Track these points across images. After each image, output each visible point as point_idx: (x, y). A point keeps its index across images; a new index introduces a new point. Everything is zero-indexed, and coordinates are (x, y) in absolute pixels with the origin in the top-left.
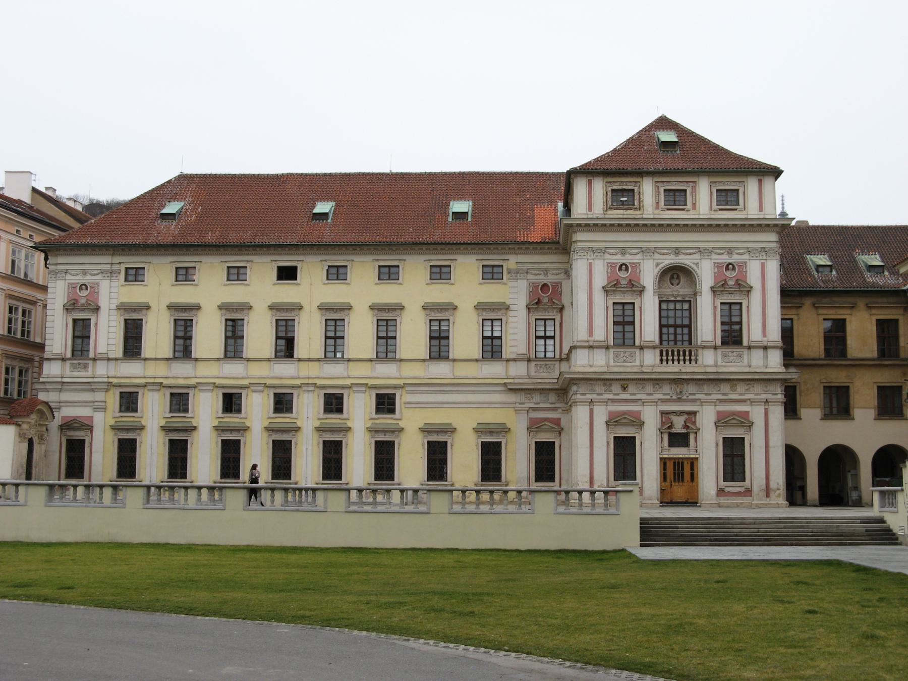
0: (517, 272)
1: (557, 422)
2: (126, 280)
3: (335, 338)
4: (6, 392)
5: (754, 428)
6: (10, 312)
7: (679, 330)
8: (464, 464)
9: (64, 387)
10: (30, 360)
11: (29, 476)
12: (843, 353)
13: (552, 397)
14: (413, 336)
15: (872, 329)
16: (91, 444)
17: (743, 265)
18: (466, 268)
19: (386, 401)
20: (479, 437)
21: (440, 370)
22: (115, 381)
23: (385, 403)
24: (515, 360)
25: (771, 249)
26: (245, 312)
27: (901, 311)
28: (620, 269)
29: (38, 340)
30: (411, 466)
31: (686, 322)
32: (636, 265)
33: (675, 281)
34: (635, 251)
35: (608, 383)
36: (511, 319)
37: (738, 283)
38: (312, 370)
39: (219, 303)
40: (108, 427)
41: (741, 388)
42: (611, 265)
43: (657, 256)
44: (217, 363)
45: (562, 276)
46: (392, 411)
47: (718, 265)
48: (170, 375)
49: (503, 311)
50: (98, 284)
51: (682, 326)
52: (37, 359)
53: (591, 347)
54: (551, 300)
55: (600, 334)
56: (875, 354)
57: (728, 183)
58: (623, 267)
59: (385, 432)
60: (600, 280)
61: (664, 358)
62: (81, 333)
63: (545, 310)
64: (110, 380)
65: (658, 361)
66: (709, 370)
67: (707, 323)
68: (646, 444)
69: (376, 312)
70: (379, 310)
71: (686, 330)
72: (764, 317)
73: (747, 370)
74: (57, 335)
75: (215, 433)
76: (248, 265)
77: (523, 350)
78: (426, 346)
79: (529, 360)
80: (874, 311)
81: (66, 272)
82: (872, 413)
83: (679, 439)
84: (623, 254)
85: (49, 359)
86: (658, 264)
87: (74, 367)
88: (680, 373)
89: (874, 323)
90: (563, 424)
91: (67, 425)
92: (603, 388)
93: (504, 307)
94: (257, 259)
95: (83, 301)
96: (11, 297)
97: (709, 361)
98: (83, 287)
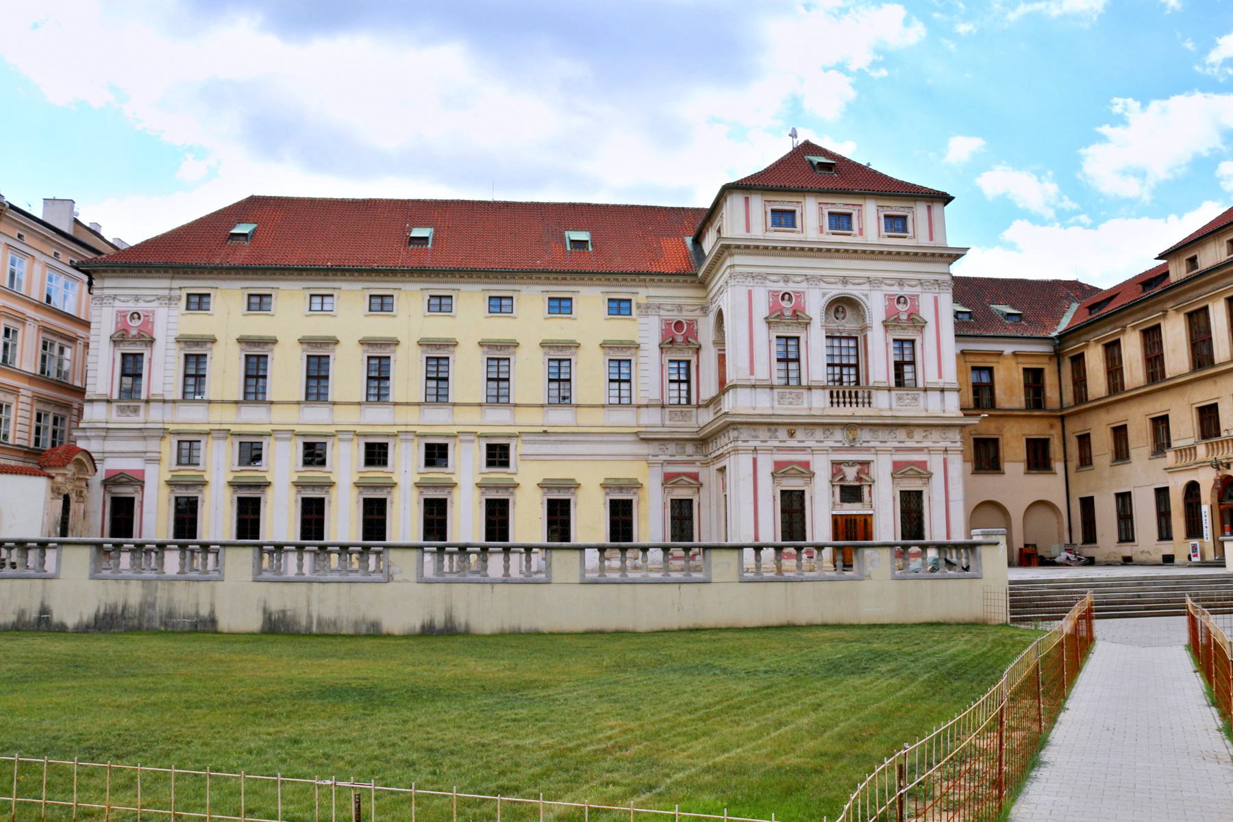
0: (648, 307)
1: (695, 476)
2: (187, 309)
3: (438, 379)
4: (37, 441)
5: (817, 479)
6: (45, 348)
7: (845, 371)
8: (589, 522)
9: (110, 434)
10: (67, 406)
11: (64, 533)
12: (992, 404)
13: (690, 449)
14: (530, 376)
15: (1019, 377)
16: (142, 503)
17: (914, 298)
18: (590, 300)
19: (498, 452)
20: (607, 494)
21: (560, 417)
22: (172, 427)
23: (498, 455)
24: (647, 406)
25: (944, 282)
26: (331, 347)
27: (1046, 360)
28: (783, 299)
29: (78, 384)
30: (528, 523)
31: (853, 361)
32: (799, 294)
33: (840, 315)
34: (798, 279)
35: (773, 428)
36: (641, 360)
37: (910, 319)
38: (410, 417)
39: (300, 337)
40: (162, 483)
41: (918, 434)
42: (774, 294)
43: (823, 285)
44: (296, 407)
45: (698, 313)
46: (506, 464)
47: (889, 298)
48: (238, 421)
49: (633, 351)
50: (153, 312)
51: (849, 366)
52: (76, 406)
53: (754, 386)
54: (687, 341)
55: (762, 373)
56: (1023, 405)
57: (896, 207)
58: (786, 296)
59: (497, 487)
60: (762, 309)
61: (835, 400)
62: (132, 368)
63: (680, 350)
64: (166, 426)
65: (828, 404)
66: (884, 414)
67: (879, 367)
68: (817, 498)
69: (486, 349)
70: (489, 346)
71: (853, 371)
72: (941, 356)
73: (924, 414)
74: (101, 371)
75: (294, 490)
76: (335, 293)
77: (655, 395)
78: (561, 386)
79: (663, 407)
80: (1020, 360)
81: (114, 298)
82: (1022, 467)
83: (851, 493)
84: (786, 281)
85: (91, 401)
86: (824, 295)
87: (122, 410)
88: (853, 416)
89: (1021, 371)
90: (701, 479)
91: (112, 480)
92: (769, 434)
93: (634, 346)
94: (345, 286)
95: (134, 332)
96: (45, 330)
97: (884, 404)
98: (136, 315)
